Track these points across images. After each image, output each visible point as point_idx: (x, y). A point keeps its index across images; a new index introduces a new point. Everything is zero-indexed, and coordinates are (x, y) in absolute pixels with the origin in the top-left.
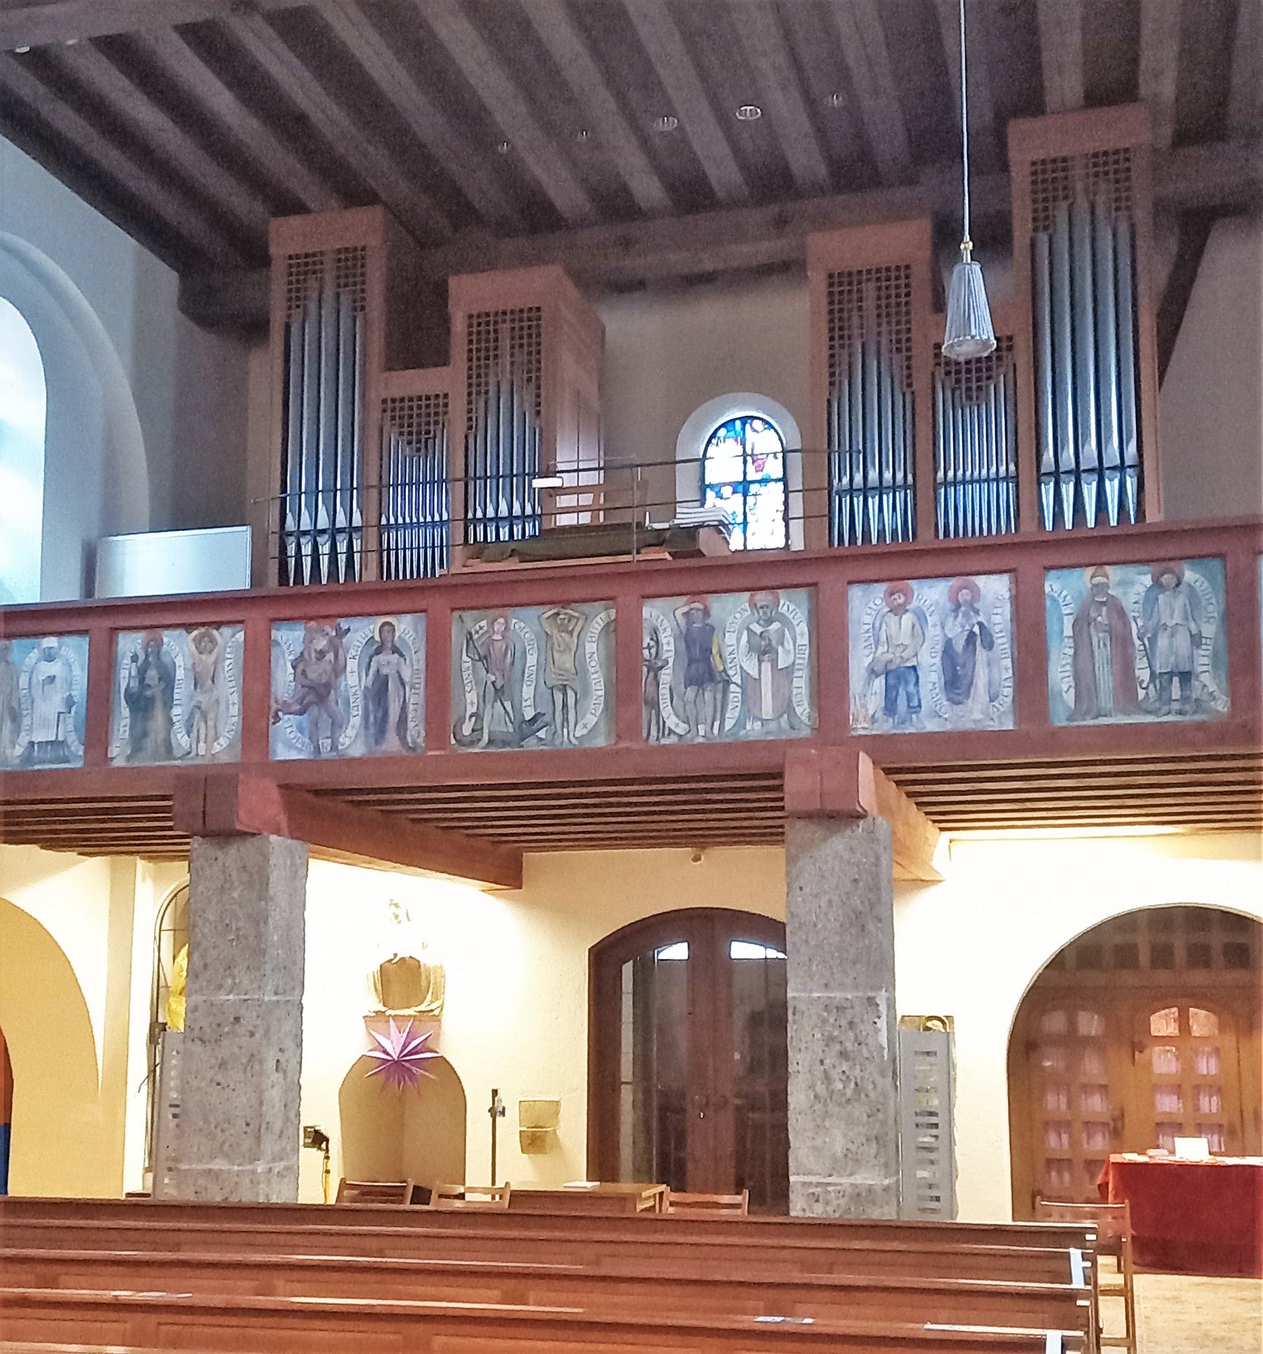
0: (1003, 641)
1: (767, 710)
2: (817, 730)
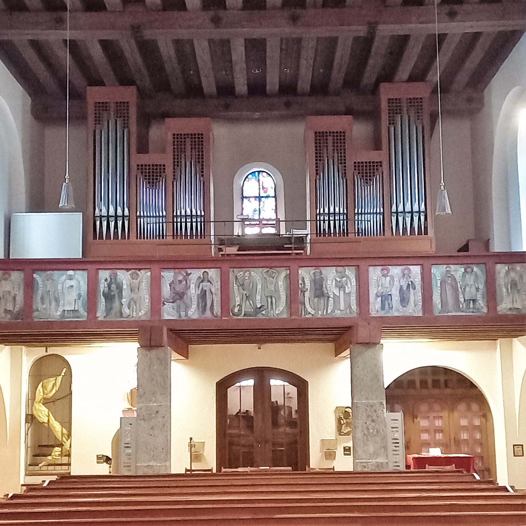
0: (418, 287)
1: (342, 307)
2: (360, 314)
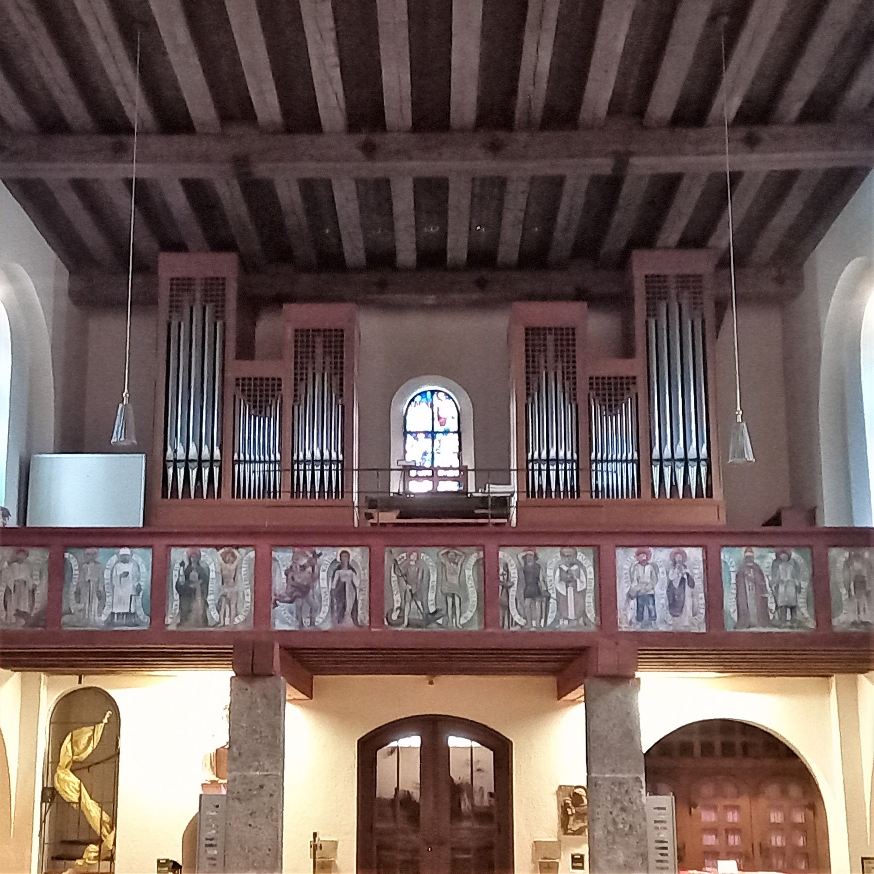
0: (699, 583)
1: (571, 614)
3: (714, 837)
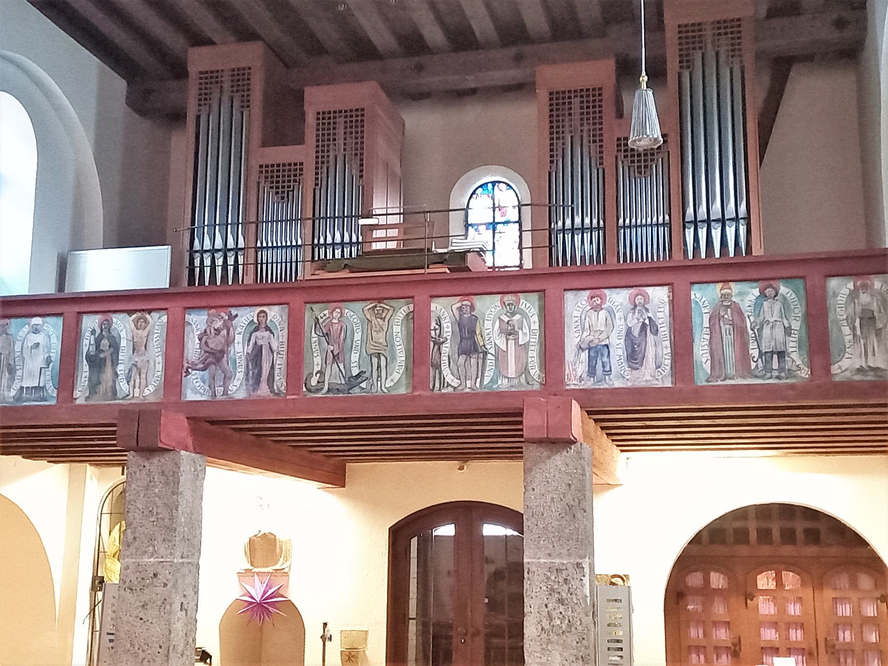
0: (664, 330)
1: (512, 371)
2: (544, 385)
3: (774, 631)
